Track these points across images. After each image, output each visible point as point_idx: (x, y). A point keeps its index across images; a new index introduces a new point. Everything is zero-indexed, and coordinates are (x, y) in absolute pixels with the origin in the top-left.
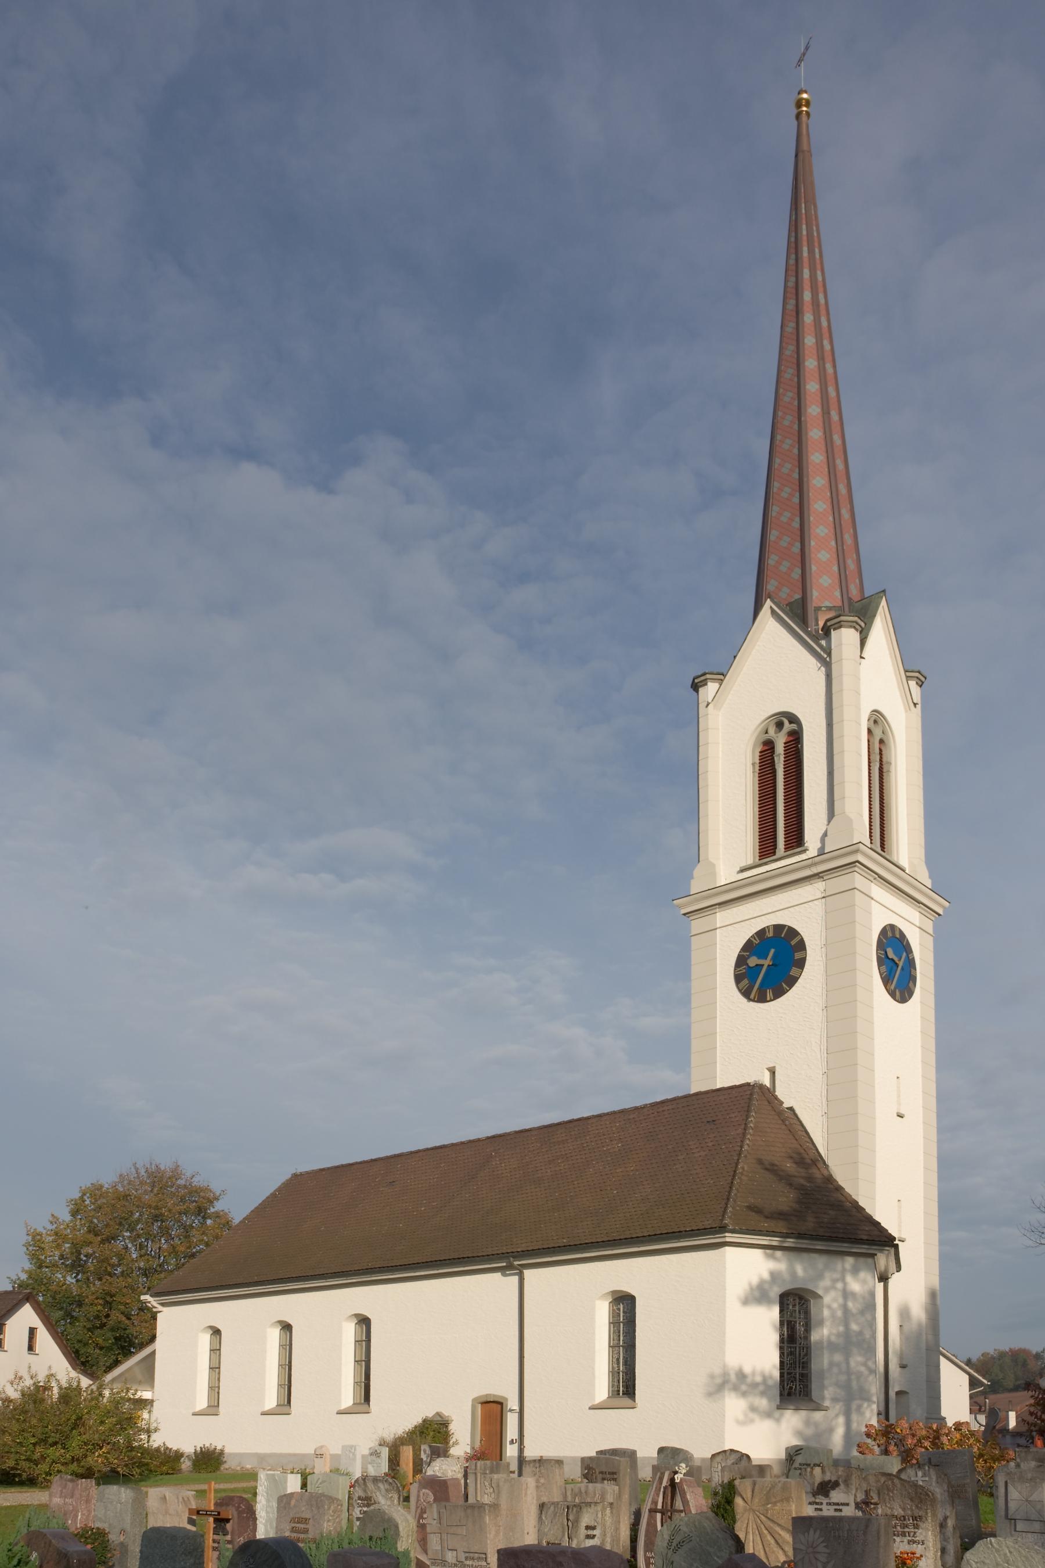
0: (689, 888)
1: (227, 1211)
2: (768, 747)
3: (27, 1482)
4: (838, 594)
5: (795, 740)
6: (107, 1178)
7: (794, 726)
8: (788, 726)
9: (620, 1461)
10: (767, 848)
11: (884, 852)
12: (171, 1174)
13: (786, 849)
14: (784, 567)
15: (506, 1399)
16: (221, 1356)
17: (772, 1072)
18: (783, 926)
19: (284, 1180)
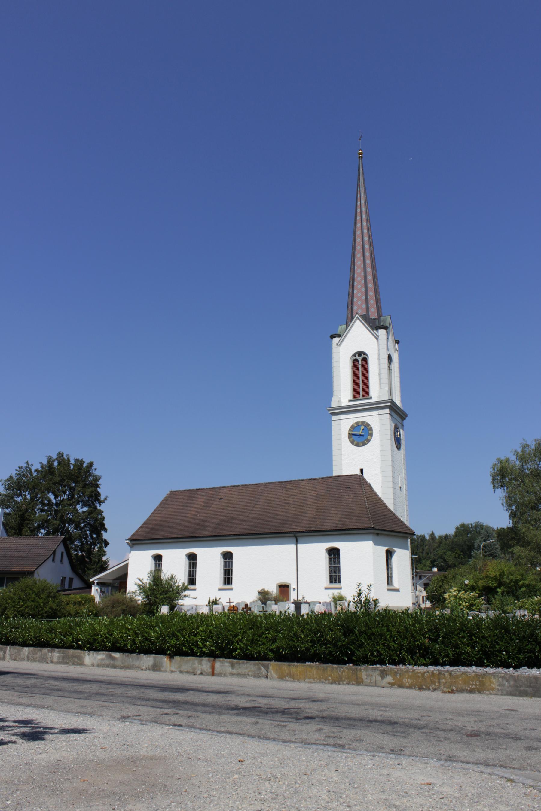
0: (330, 404)
1: (102, 498)
2: (355, 361)
3: (46, 600)
4: (376, 314)
5: (365, 360)
6: (466, 523)
7: (357, 355)
8: (363, 356)
9: (3, 586)
10: (356, 394)
11: (371, 398)
12: (17, 477)
13: (363, 396)
14: (360, 303)
15: (290, 584)
16: (386, 577)
17: (362, 471)
18: (365, 422)
19: (491, 526)
